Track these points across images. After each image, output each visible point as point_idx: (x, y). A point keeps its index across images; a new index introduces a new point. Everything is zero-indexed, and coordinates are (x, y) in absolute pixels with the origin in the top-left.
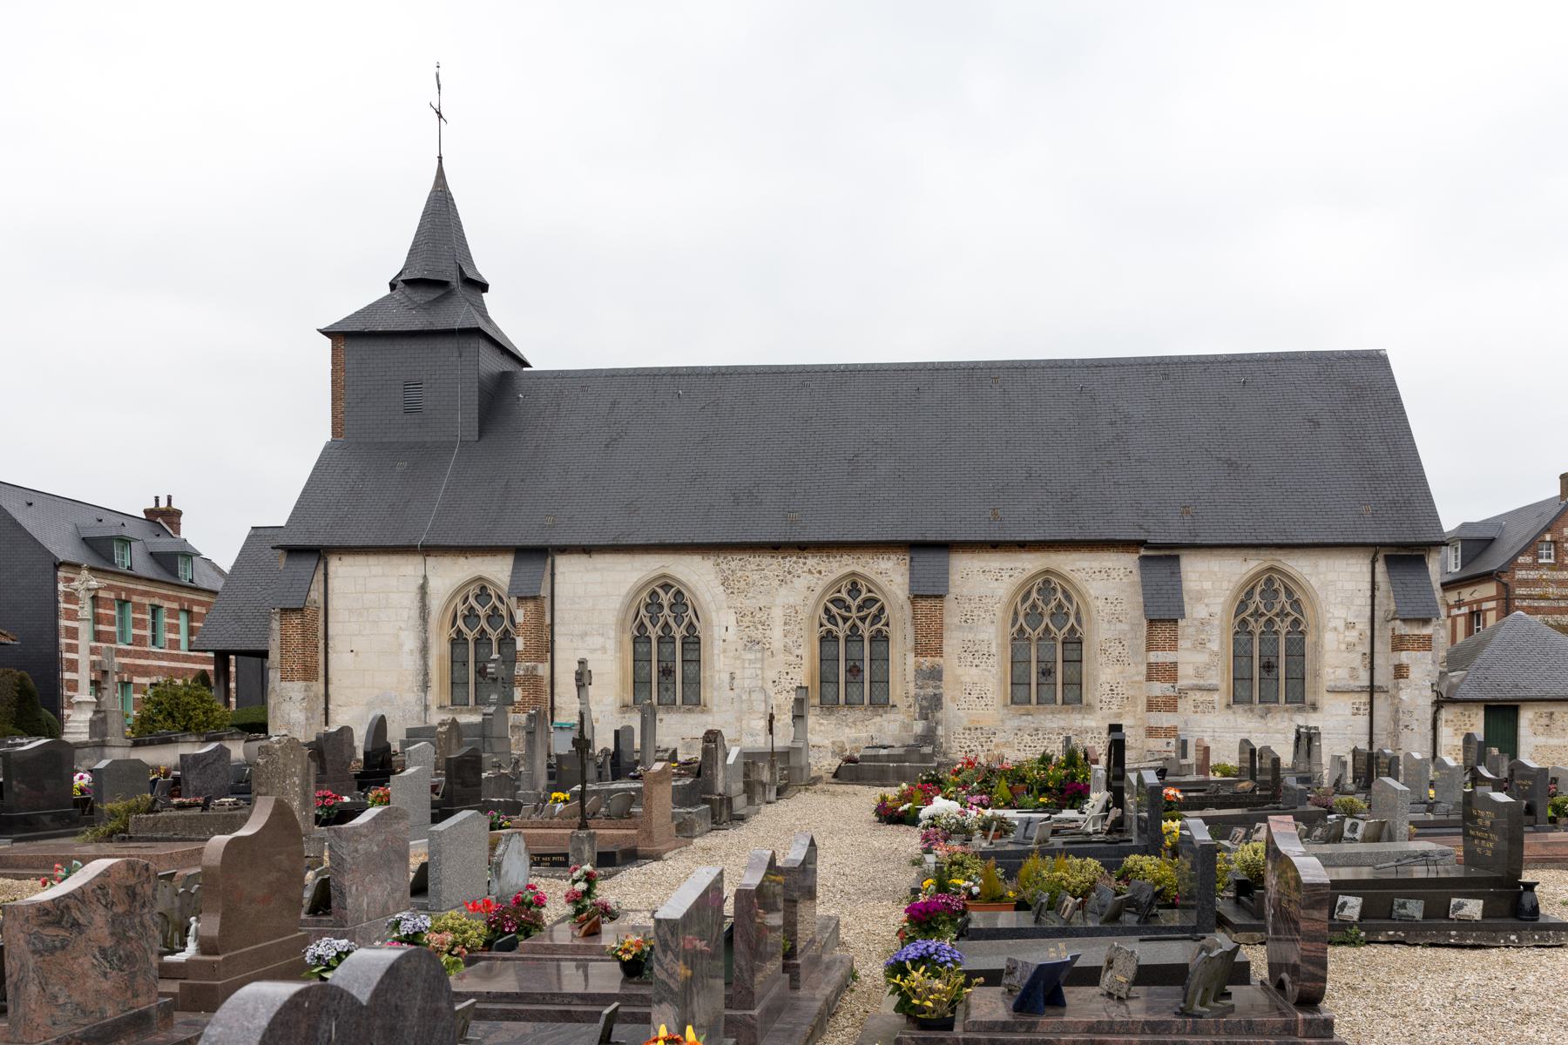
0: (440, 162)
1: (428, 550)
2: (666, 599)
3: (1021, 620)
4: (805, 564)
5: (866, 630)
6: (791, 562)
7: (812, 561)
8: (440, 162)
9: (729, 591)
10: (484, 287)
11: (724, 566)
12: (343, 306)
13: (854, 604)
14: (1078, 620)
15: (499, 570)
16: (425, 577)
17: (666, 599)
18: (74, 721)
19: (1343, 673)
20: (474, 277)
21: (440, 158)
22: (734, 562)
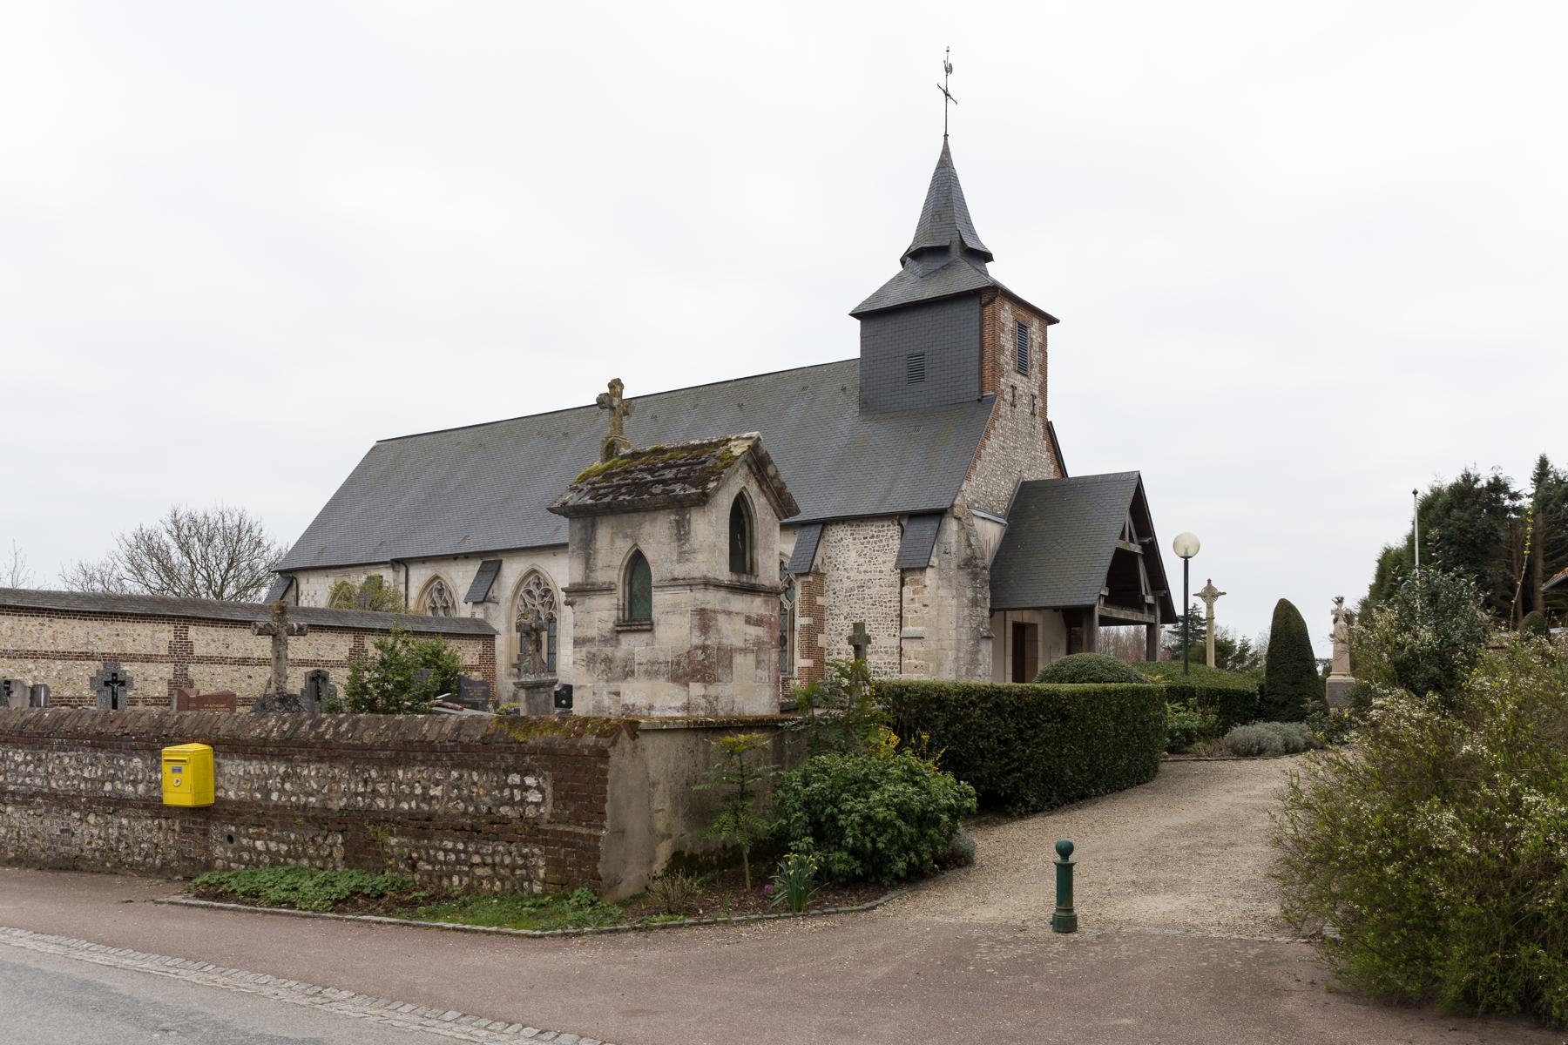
0: (946, 139)
8: (946, 139)
10: (987, 257)
20: (975, 246)
21: (946, 135)
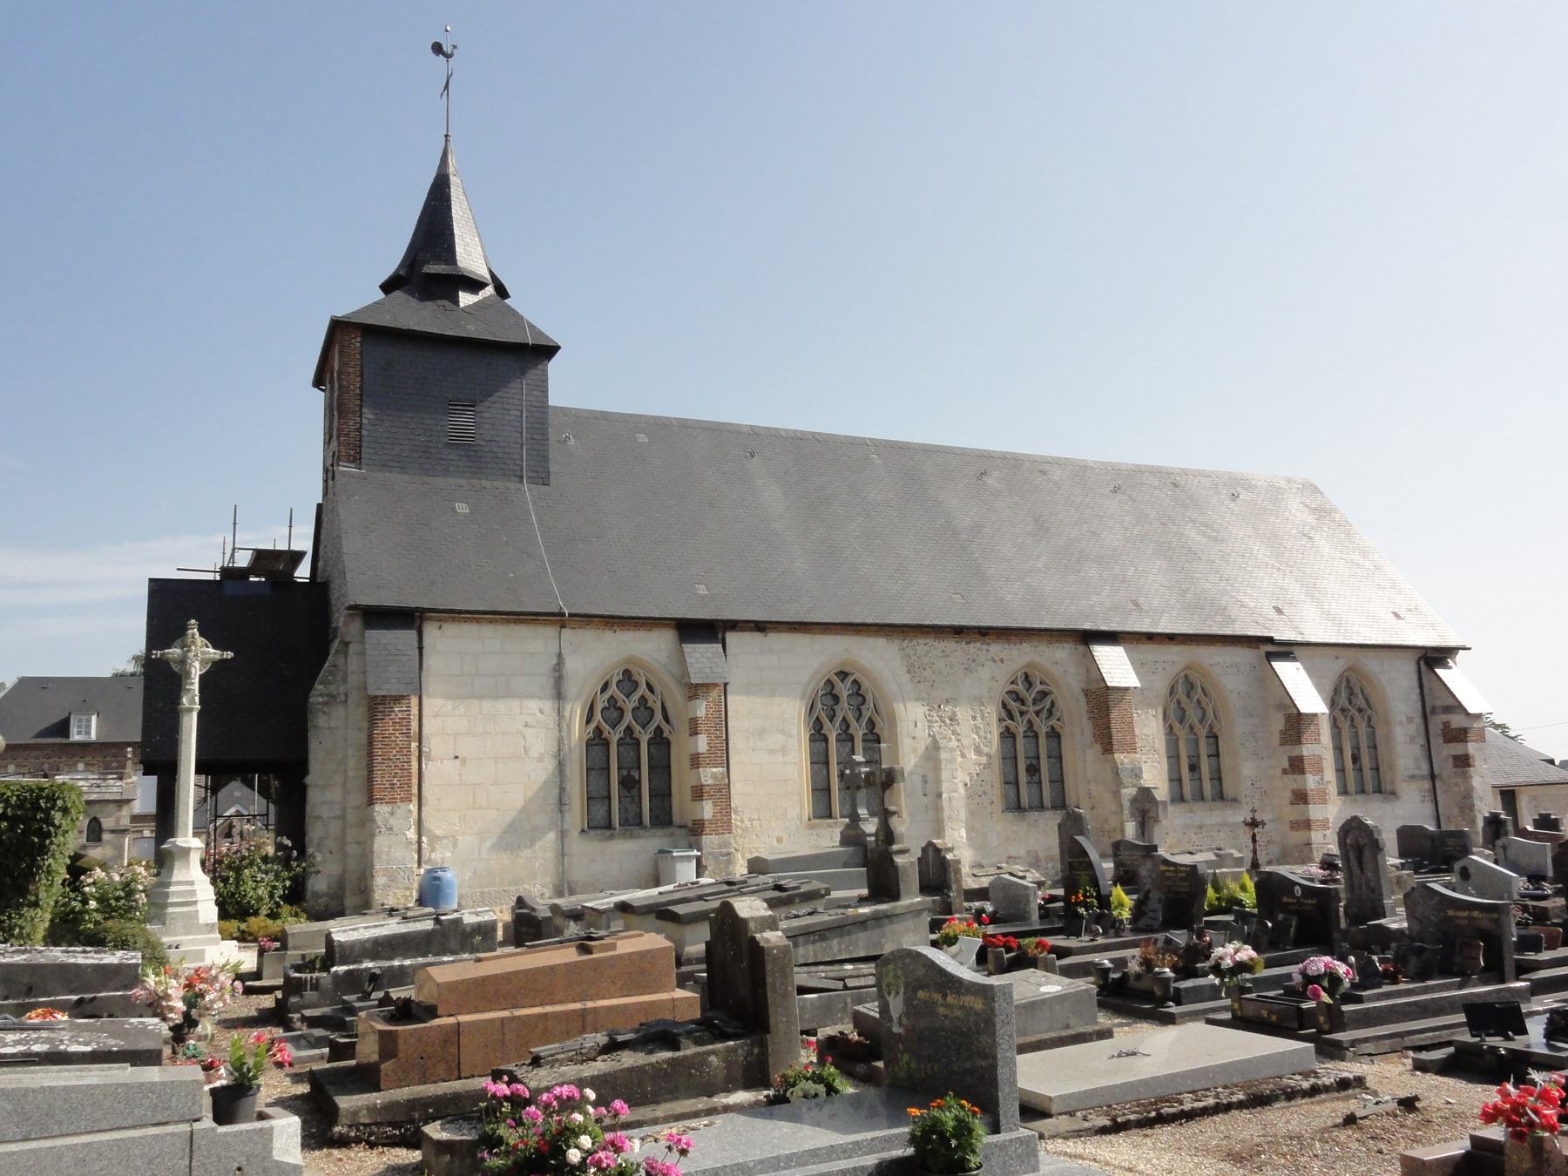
1: (558, 619)
2: (844, 690)
3: (598, 716)
4: (988, 651)
5: (1042, 728)
6: (975, 648)
7: (996, 648)
9: (916, 680)
11: (909, 651)
12: (343, 310)
13: (1030, 699)
14: (666, 718)
15: (654, 648)
16: (560, 655)
17: (844, 690)
18: (180, 883)
19: (1411, 764)
22: (923, 647)
